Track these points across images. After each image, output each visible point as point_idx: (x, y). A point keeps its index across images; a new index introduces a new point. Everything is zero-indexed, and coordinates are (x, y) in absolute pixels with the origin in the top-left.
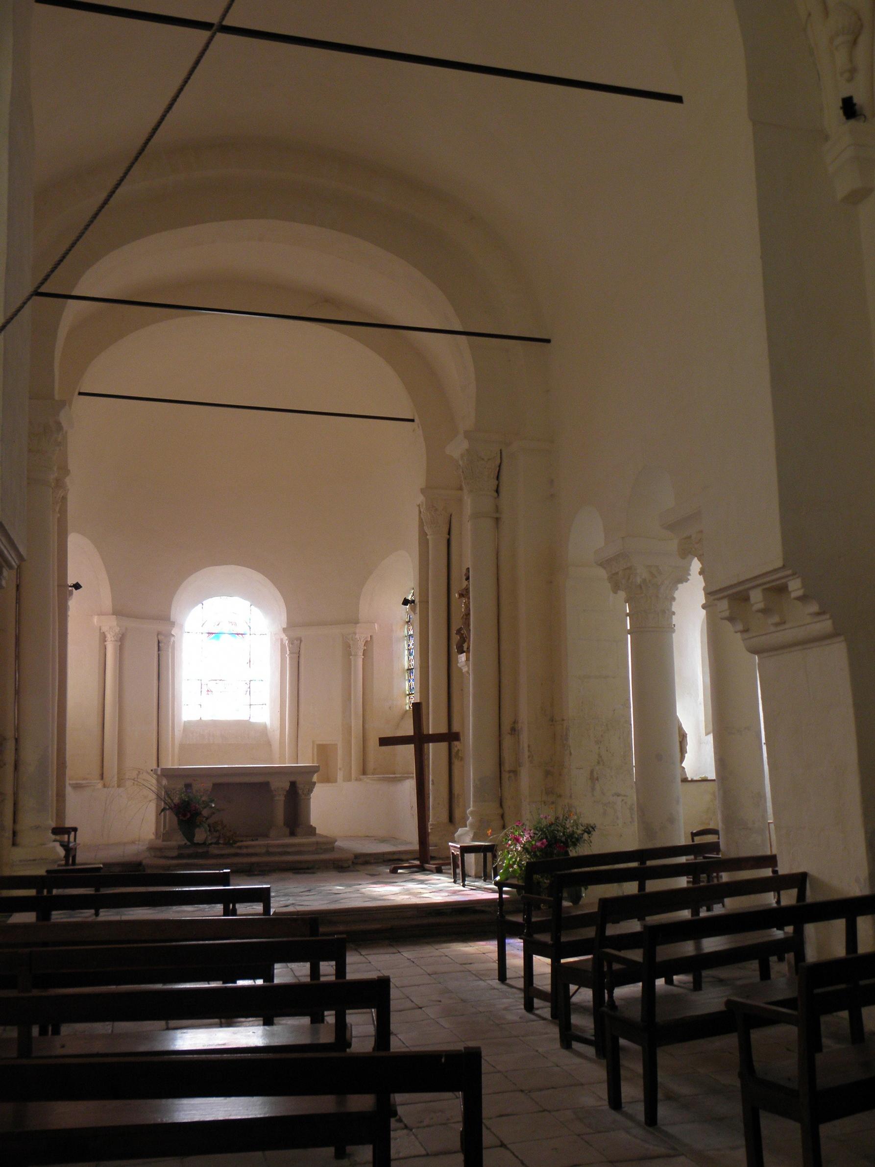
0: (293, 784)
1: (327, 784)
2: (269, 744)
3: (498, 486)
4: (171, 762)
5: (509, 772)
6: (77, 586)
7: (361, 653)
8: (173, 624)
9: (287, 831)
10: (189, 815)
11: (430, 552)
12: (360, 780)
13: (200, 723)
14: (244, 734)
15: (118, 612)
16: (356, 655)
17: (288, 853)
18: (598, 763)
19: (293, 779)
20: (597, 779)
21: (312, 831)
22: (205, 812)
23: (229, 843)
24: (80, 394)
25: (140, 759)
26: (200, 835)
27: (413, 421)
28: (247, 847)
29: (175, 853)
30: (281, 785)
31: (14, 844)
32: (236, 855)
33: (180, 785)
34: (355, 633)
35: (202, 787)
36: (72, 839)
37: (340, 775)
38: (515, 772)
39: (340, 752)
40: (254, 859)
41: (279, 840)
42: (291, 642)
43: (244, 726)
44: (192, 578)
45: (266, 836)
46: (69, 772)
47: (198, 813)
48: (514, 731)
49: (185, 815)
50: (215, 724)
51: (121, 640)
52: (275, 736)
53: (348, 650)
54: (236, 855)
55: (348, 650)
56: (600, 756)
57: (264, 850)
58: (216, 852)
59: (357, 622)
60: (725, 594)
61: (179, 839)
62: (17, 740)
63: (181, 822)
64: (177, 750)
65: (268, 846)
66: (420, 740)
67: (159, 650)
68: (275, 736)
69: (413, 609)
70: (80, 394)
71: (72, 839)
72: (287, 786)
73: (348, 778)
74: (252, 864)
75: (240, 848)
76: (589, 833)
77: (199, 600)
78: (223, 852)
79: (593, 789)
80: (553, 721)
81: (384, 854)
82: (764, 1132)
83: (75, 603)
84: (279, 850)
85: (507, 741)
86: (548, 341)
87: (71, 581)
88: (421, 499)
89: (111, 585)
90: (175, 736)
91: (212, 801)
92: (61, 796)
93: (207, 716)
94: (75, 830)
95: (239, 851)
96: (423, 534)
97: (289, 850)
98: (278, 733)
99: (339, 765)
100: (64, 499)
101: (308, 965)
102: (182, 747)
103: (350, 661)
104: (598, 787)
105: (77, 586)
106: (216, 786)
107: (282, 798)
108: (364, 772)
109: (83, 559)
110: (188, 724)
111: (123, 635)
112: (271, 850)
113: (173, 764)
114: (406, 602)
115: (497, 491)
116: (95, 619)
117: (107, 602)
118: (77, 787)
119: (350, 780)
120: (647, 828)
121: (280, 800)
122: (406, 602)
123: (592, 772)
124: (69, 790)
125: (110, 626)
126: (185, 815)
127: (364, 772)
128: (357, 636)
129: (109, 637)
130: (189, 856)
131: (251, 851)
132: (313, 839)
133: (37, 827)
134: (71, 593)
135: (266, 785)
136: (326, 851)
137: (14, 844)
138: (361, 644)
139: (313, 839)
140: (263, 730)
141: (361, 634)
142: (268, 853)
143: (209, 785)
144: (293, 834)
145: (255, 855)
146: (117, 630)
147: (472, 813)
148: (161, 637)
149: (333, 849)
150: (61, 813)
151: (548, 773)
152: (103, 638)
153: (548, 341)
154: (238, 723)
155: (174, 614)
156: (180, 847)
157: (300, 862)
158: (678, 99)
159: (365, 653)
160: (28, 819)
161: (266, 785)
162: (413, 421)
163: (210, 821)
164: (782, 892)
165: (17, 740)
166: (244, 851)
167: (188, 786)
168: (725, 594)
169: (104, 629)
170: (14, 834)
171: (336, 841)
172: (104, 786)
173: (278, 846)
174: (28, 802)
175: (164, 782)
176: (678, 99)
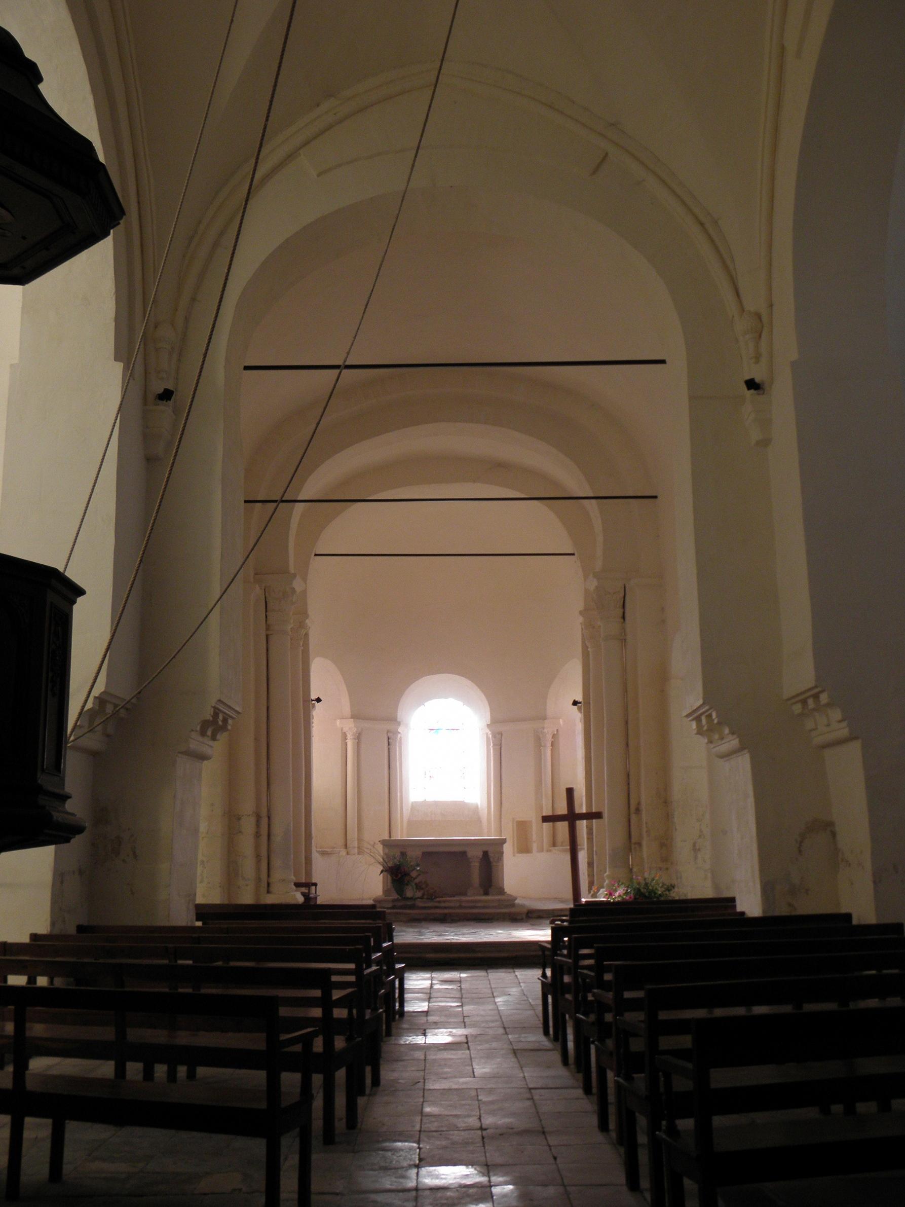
0: (486, 854)
1: (525, 855)
2: (479, 820)
3: (624, 613)
4: (400, 835)
5: (635, 843)
6: (318, 700)
7: (549, 744)
8: (399, 724)
9: (482, 891)
11: (591, 662)
13: (425, 803)
14: (460, 813)
15: (355, 716)
16: (545, 746)
18: (700, 837)
19: (485, 849)
20: (699, 850)
21: (501, 891)
22: (414, 874)
23: (431, 897)
24: (316, 555)
25: (375, 833)
27: (573, 554)
28: (444, 902)
29: (390, 905)
30: (475, 854)
31: (268, 892)
32: (436, 907)
34: (543, 728)
35: (414, 854)
36: (313, 891)
37: (535, 846)
38: (639, 844)
39: (534, 827)
40: (446, 911)
41: (474, 897)
42: (494, 736)
43: (459, 807)
45: (465, 894)
47: (406, 874)
48: (638, 810)
49: (397, 876)
50: (436, 804)
51: (358, 738)
52: (484, 814)
54: (436, 907)
56: (701, 831)
57: (458, 904)
59: (544, 718)
60: (797, 699)
61: (395, 896)
62: (269, 818)
63: (393, 881)
66: (572, 817)
67: (389, 744)
68: (484, 814)
69: (579, 709)
70: (316, 555)
71: (313, 891)
72: (480, 854)
73: (541, 850)
74: (446, 914)
75: (439, 902)
76: (669, 891)
77: (421, 701)
78: (426, 905)
79: (696, 858)
80: (665, 801)
81: (553, 910)
83: (318, 713)
85: (634, 818)
86: (656, 497)
87: (313, 697)
88: (581, 619)
89: (350, 696)
90: (404, 813)
91: (418, 865)
92: (308, 860)
93: (430, 798)
94: (315, 885)
96: (585, 648)
98: (486, 811)
99: (534, 837)
100: (307, 635)
102: (410, 822)
103: (540, 752)
104: (699, 856)
105: (318, 700)
106: (424, 854)
107: (477, 864)
108: (554, 845)
109: (325, 678)
110: (415, 806)
111: (360, 734)
112: (463, 904)
113: (402, 836)
114: (575, 703)
115: (624, 617)
116: (338, 722)
117: (347, 709)
118: (323, 853)
119: (542, 851)
120: (716, 886)
121: (476, 866)
122: (575, 703)
123: (694, 845)
124: (315, 856)
125: (350, 727)
126: (397, 876)
127: (554, 845)
128: (546, 730)
129: (349, 736)
130: (401, 907)
131: (446, 904)
132: (502, 897)
134: (314, 706)
136: (506, 907)
137: (268, 892)
138: (549, 738)
139: (502, 897)
140: (475, 810)
141: (549, 729)
142: (461, 907)
143: (418, 853)
144: (486, 893)
146: (355, 730)
147: (608, 876)
149: (513, 905)
150: (309, 873)
151: (662, 845)
153: (656, 497)
154: (455, 803)
155: (401, 714)
156: (394, 901)
157: (483, 914)
158: (663, 362)
160: (277, 875)
162: (573, 554)
163: (417, 881)
165: (269, 818)
166: (443, 905)
167: (403, 854)
168: (797, 699)
169: (345, 730)
170: (268, 884)
171: (516, 899)
172: (348, 853)
173: (468, 901)
174: (277, 862)
175: (387, 851)
176: (663, 362)
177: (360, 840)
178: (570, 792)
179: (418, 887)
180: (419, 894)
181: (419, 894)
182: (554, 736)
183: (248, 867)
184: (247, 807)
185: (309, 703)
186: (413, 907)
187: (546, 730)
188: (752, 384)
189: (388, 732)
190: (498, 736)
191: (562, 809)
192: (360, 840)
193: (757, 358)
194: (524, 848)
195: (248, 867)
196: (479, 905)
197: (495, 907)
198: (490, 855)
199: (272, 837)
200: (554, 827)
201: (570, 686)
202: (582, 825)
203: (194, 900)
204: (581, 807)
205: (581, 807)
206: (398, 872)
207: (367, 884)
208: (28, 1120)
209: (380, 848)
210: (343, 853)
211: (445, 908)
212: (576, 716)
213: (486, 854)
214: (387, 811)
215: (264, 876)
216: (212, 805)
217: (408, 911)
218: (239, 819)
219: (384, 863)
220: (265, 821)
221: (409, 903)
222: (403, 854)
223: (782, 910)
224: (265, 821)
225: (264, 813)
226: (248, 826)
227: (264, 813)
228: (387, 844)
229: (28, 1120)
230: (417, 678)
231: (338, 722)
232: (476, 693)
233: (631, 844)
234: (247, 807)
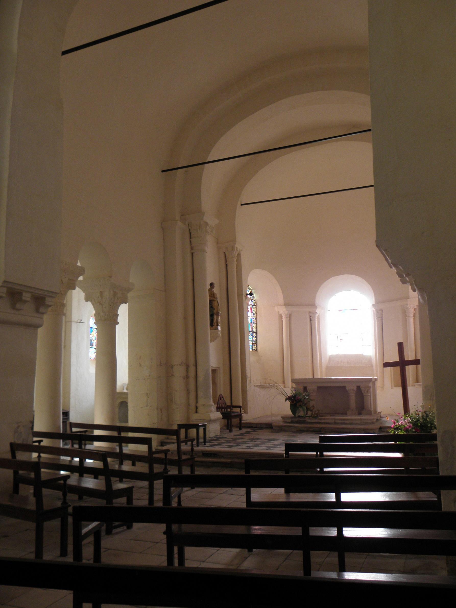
0: (359, 387)
2: (372, 366)
10: (295, 402)
12: (414, 386)
13: (338, 356)
15: (286, 304)
17: (346, 424)
19: (358, 385)
24: (242, 205)
28: (324, 419)
29: (290, 420)
33: (301, 387)
34: (407, 304)
43: (359, 358)
44: (326, 283)
45: (345, 414)
50: (345, 356)
51: (290, 317)
57: (333, 421)
58: (309, 421)
64: (324, 370)
65: (335, 419)
66: (402, 364)
67: (311, 320)
70: (242, 205)
72: (355, 388)
74: (321, 428)
75: (321, 419)
78: (313, 421)
84: (340, 422)
95: (320, 421)
97: (346, 422)
98: (375, 359)
101: (244, 489)
102: (327, 368)
106: (319, 388)
107: (354, 395)
110: (331, 358)
112: (337, 421)
113: (321, 376)
116: (276, 308)
117: (281, 301)
121: (353, 396)
125: (283, 310)
128: (409, 306)
129: (284, 316)
130: (296, 422)
133: (204, 405)
135: (344, 387)
137: (196, 412)
140: (370, 359)
142: (335, 423)
144: (360, 414)
145: (322, 423)
146: (287, 312)
148: (311, 314)
152: (281, 316)
155: (318, 301)
157: (337, 428)
161: (344, 387)
164: (443, 492)
166: (323, 421)
167: (305, 389)
169: (281, 313)
173: (341, 419)
175: (294, 386)
183: (179, 397)
184: (178, 357)
186: (304, 422)
187: (409, 306)
189: (310, 313)
190: (380, 312)
195: (179, 397)
196: (348, 422)
197: (359, 424)
198: (362, 389)
199: (198, 378)
200: (417, 368)
202: (410, 369)
203: (32, 428)
205: (409, 355)
206: (295, 402)
208: (252, 489)
211: (322, 423)
213: (359, 387)
214: (310, 362)
215: (192, 402)
216: (152, 359)
217: (295, 425)
218: (172, 367)
220: (192, 369)
221: (301, 420)
222: (305, 389)
224: (192, 369)
225: (192, 362)
226: (179, 372)
228: (293, 381)
229: (252, 489)
230: (327, 279)
231: (276, 308)
232: (367, 286)
234: (178, 357)
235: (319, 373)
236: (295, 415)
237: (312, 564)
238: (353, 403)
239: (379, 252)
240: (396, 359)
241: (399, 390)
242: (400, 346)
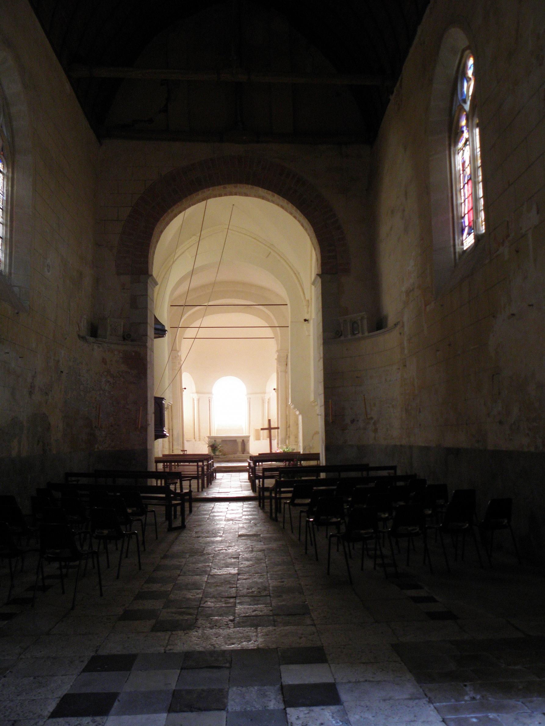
0: (243, 440)
4: (214, 434)
6: (185, 389)
15: (197, 393)
22: (219, 447)
23: (224, 455)
25: (205, 434)
26: (217, 453)
31: (127, 557)
35: (219, 441)
37: (261, 438)
41: (239, 455)
46: (185, 437)
47: (216, 447)
48: (289, 427)
51: (199, 400)
53: (263, 402)
55: (263, 402)
63: (212, 450)
66: (270, 429)
72: (241, 441)
73: (264, 439)
82: (241, 474)
83: (185, 392)
87: (183, 387)
92: (183, 443)
96: (277, 370)
105: (185, 389)
106: (458, 133)
109: (187, 380)
114: (274, 389)
117: (194, 390)
118: (188, 441)
121: (240, 445)
122: (274, 389)
124: (185, 441)
125: (196, 396)
138: (267, 400)
143: (220, 440)
144: (243, 453)
150: (183, 447)
159: (268, 402)
167: (215, 441)
174: (175, 443)
177: (199, 436)
178: (269, 421)
179: (220, 451)
180: (220, 454)
181: (220, 454)
182: (269, 399)
185: (182, 390)
186: (218, 458)
188: (305, 320)
191: (266, 426)
192: (199, 436)
193: (308, 312)
194: (258, 438)
201: (273, 383)
204: (273, 425)
206: (213, 447)
207: (205, 450)
209: (207, 438)
210: (194, 440)
212: (274, 394)
213: (243, 440)
219: (209, 442)
220: (171, 431)
222: (215, 441)
223: (307, 452)
227: (171, 428)
233: (287, 436)
235: (464, 716)
236: (214, 453)
237: (81, 718)
238: (240, 448)
239: (212, 712)
240: (266, 426)
241: (268, 439)
242: (269, 421)
